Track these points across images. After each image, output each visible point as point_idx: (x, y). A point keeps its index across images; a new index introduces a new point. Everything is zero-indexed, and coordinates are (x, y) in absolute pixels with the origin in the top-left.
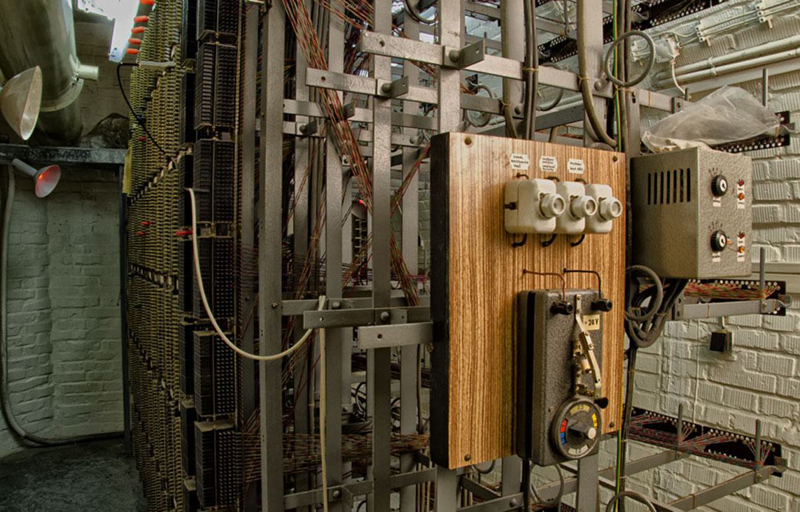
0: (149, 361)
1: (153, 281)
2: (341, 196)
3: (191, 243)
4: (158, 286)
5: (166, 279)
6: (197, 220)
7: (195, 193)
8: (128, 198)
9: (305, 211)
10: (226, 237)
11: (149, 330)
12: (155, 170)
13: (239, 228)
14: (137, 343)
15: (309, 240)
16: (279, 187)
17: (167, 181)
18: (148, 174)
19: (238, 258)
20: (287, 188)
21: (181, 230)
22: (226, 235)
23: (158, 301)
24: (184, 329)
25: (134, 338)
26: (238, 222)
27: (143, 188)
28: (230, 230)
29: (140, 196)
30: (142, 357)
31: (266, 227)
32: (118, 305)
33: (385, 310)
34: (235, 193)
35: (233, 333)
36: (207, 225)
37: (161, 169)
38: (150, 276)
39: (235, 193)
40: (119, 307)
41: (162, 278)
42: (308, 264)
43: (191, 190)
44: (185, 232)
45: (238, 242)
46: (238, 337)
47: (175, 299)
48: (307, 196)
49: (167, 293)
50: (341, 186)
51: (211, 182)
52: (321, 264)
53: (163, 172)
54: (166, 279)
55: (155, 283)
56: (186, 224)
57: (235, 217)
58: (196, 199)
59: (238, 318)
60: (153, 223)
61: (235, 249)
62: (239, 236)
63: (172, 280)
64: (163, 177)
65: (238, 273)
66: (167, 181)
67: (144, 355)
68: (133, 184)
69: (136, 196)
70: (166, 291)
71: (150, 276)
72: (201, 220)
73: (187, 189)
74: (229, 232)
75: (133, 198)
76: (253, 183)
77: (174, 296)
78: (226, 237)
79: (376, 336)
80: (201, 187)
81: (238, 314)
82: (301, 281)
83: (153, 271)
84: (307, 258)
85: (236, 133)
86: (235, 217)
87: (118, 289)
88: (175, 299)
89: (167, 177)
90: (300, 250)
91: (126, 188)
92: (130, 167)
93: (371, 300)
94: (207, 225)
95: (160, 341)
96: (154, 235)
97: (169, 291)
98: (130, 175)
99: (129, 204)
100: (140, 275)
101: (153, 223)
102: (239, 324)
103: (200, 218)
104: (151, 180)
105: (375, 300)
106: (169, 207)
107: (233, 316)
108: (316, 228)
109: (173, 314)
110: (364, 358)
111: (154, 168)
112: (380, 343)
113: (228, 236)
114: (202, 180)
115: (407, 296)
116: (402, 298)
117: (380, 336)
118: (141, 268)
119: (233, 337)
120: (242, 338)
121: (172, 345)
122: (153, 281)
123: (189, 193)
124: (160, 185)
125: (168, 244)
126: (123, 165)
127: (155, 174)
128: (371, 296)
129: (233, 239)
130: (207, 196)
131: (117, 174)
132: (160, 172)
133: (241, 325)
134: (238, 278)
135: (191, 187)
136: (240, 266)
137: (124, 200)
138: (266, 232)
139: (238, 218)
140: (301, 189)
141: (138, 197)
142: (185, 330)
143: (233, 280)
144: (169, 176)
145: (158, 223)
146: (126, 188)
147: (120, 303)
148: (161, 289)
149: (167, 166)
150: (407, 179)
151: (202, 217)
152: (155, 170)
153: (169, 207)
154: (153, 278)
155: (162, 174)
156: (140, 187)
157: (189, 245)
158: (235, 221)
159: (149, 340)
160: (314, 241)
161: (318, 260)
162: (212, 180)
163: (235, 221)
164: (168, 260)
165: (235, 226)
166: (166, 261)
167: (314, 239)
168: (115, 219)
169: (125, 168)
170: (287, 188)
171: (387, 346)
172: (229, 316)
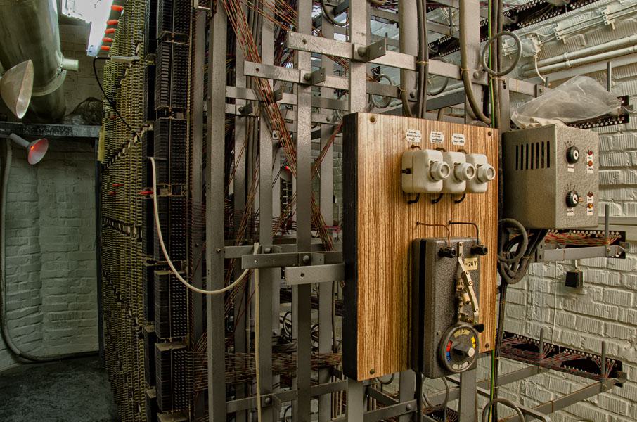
0: (118, 295)
1: (122, 231)
3: (152, 200)
5: (132, 229)
7: (155, 160)
13: (190, 189)
14: (109, 280)
15: (246, 198)
19: (190, 212)
20: (229, 157)
21: (144, 191)
25: (106, 277)
26: (190, 184)
29: (112, 164)
30: (113, 292)
31: (212, 188)
33: (307, 254)
34: (187, 161)
37: (128, 142)
43: (152, 159)
44: (147, 192)
45: (190, 200)
46: (189, 276)
47: (140, 245)
48: (244, 163)
54: (132, 229)
55: (123, 233)
57: (187, 180)
59: (190, 260)
62: (190, 195)
66: (133, 151)
67: (115, 290)
68: (106, 154)
74: (182, 192)
76: (201, 153)
80: (160, 156)
81: (190, 257)
83: (121, 223)
86: (187, 180)
90: (238, 206)
98: (104, 146)
102: (190, 265)
103: (159, 180)
107: (185, 259)
113: (182, 195)
118: (112, 220)
121: (137, 282)
122: (122, 231)
123: (150, 161)
126: (98, 139)
127: (123, 146)
129: (185, 197)
134: (190, 228)
135: (152, 156)
137: (98, 167)
139: (190, 181)
140: (240, 157)
142: (148, 270)
143: (185, 230)
148: (128, 238)
149: (133, 139)
155: (129, 146)
156: (111, 156)
158: (187, 183)
160: (250, 199)
161: (253, 215)
163: (187, 183)
164: (134, 214)
165: (187, 187)
166: (132, 215)
170: (229, 157)
172: (183, 259)
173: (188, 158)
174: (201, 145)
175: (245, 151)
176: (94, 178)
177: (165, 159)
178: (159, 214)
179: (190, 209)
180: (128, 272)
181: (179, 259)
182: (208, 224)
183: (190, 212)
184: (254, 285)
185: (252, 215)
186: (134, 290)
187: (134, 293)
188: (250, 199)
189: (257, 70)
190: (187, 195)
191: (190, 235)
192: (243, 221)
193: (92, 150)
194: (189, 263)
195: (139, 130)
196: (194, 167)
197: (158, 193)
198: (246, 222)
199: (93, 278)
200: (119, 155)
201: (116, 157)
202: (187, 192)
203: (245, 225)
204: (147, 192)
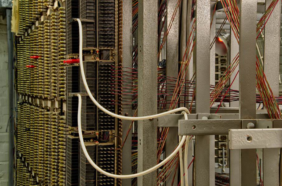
0: (34, 177)
1: (41, 106)
2: (209, 22)
3: (78, 67)
4: (46, 110)
5: (53, 104)
6: (83, 47)
7: (83, 23)
8: (16, 37)
9: (176, 40)
10: (108, 61)
11: (37, 149)
12: (41, 10)
13: (120, 53)
14: (24, 162)
15: (180, 65)
16: (155, 16)
17: (53, 18)
18: (35, 14)
19: (119, 79)
20: (161, 26)
21: (68, 57)
22: (109, 60)
23: (46, 122)
24: (71, 141)
25: (21, 158)
26: (119, 48)
27: (30, 27)
28: (112, 55)
29: (28, 35)
30: (29, 174)
31: (144, 50)
32: (7, 131)
33: (250, 121)
34: (116, 23)
35: (114, 144)
36: (92, 51)
37: (47, 8)
38: (38, 103)
39: (116, 23)
40: (7, 134)
41: (49, 104)
42: (179, 85)
43: (79, 20)
44: (71, 60)
45: (119, 65)
46: (119, 147)
47: (62, 119)
48: (178, 26)
49: (54, 115)
50: (209, 13)
51: (96, 14)
52: (190, 85)
53: (49, 11)
54: (53, 104)
55: (43, 108)
56: (73, 52)
57: (116, 44)
58: (83, 28)
59: (119, 130)
60: (41, 56)
61: (117, 72)
62: (120, 61)
63: (59, 104)
64: (49, 16)
65: (119, 89)
66: (53, 18)
67: (31, 172)
68: (20, 24)
69: (24, 35)
70: (54, 113)
71: (38, 103)
72: (87, 46)
73: (75, 19)
74: (111, 58)
75: (21, 37)
76: (131, 14)
77: (61, 117)
78: (108, 61)
79: (246, 138)
80: (87, 17)
81: (119, 127)
82: (172, 99)
83: (41, 98)
84: (178, 80)
85: (34, 101)
86: (116, 44)
87: (7, 117)
88: (62, 119)
89: (53, 15)
90: (171, 73)
91: (15, 28)
92: (17, 9)
93: (238, 115)
94: (92, 51)
95: (47, 158)
96: (42, 67)
97: (56, 113)
98: (17, 16)
99: (17, 42)
100: (29, 103)
101: (41, 56)
102: (119, 136)
103: (86, 44)
104: (38, 19)
105: (241, 115)
106: (56, 41)
107: (114, 129)
108: (186, 53)
109: (60, 132)
110: (227, 178)
111: (40, 8)
112: (249, 145)
113: (110, 61)
114: (88, 11)
115: (270, 113)
116: (267, 114)
117: (249, 138)
118: (29, 96)
119: (114, 147)
120: (122, 149)
121: (58, 159)
122: (41, 106)
123: (77, 23)
124: (46, 22)
125: (54, 73)
126: (11, 9)
127: (41, 14)
128: (238, 113)
129: (114, 63)
130: (92, 25)
131: (4, 17)
132: (47, 12)
133: (121, 136)
134: (119, 96)
135: (78, 17)
136: (120, 86)
137: (11, 39)
138: (144, 54)
139: (119, 45)
140: (173, 19)
141: (26, 35)
142: (73, 143)
143: (114, 97)
144: (56, 13)
145: (46, 55)
146: (15, 28)
147: (8, 131)
148: (49, 113)
149: (53, 5)
150: (270, 7)
151: (89, 43)
152: (41, 10)
153: (56, 41)
154: (41, 104)
155: (48, 13)
156: (27, 28)
157: (76, 71)
158: (116, 48)
159: (37, 157)
160: (184, 65)
161: (187, 82)
162: (96, 11)
163: (116, 48)
164: (55, 86)
165: (116, 52)
166: (53, 88)
167: (184, 63)
168: (3, 56)
169: (13, 10)
170: (161, 26)
171: (255, 148)
172: (111, 129)
173: (117, 20)
174: (131, 6)
175: (178, 12)
176: (7, 54)
177: (92, 21)
178: (87, 80)
179: (120, 75)
180: (48, 150)
181: (108, 129)
182: (140, 88)
183: (119, 79)
184: (184, 4)
185: (185, 83)
186: (54, 169)
187: (54, 172)
188: (184, 65)
189: (249, 138)
190: (116, 61)
191: (120, 103)
192: (176, 89)
193: (3, 22)
194: (118, 134)
195: (45, 10)
196: (123, 36)
197: (83, 60)
198: (179, 91)
199: (5, 163)
200: (33, 29)
201: (29, 31)
202: (116, 57)
203: (179, 93)
204: (71, 60)
